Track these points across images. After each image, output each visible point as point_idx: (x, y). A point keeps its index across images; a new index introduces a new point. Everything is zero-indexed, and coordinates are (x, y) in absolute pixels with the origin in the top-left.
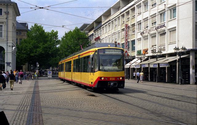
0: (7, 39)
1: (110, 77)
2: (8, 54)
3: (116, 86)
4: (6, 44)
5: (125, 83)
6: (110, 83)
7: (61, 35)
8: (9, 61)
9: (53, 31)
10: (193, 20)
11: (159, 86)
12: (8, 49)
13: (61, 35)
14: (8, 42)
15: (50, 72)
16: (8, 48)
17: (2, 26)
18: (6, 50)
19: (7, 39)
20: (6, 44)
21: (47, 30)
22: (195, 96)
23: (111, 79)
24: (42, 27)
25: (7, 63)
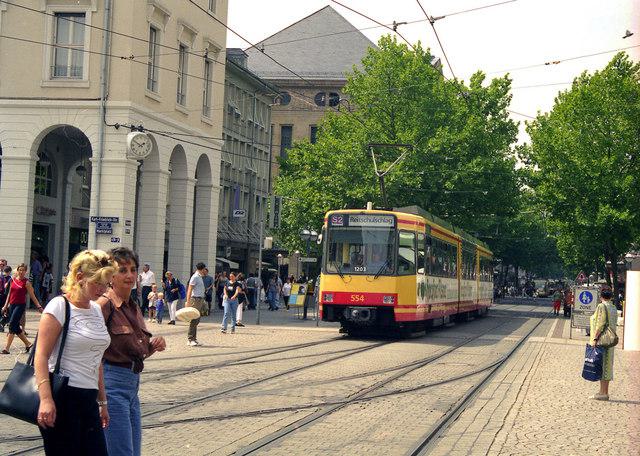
0: (106, 84)
1: (383, 294)
2: (105, 171)
3: (368, 318)
4: (96, 112)
6: (351, 311)
7: (530, 104)
8: (105, 213)
9: (479, 77)
10: (227, 12)
12: (108, 146)
13: (530, 104)
14: (109, 103)
16: (108, 138)
17: (83, 15)
18: (95, 147)
19: (106, 84)
20: (97, 120)
21: (458, 68)
22: (638, 400)
23: (226, 214)
25: (99, 221)
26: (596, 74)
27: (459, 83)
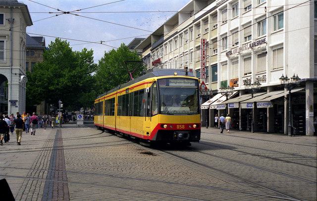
0: (12, 62)
1: (177, 124)
2: (13, 87)
3: (187, 138)
4: (9, 70)
5: (201, 134)
6: (177, 134)
7: (98, 57)
8: (14, 99)
9: (85, 50)
12: (13, 80)
13: (98, 57)
14: (13, 67)
15: (81, 116)
16: (13, 77)
17: (3, 41)
18: (9, 80)
19: (12, 62)
20: (9, 71)
21: (76, 48)
22: (314, 155)
25: (11, 101)
26: (106, 55)
27: (68, 43)
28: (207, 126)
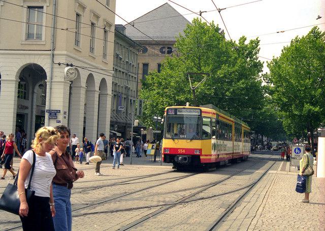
0: (54, 43)
2: (53, 87)
3: (187, 161)
4: (49, 57)
5: (12, 120)
6: (178, 157)
7: (269, 53)
8: (53, 108)
9: (243, 39)
11: (90, 212)
12: (55, 74)
13: (269, 53)
14: (56, 52)
15: (299, 149)
16: (55, 70)
17: (42, 7)
18: (48, 74)
19: (54, 43)
20: (49, 61)
21: (233, 35)
22: (324, 203)
23: (115, 108)
24: (233, 42)
25: (50, 112)
28: (94, 92)
